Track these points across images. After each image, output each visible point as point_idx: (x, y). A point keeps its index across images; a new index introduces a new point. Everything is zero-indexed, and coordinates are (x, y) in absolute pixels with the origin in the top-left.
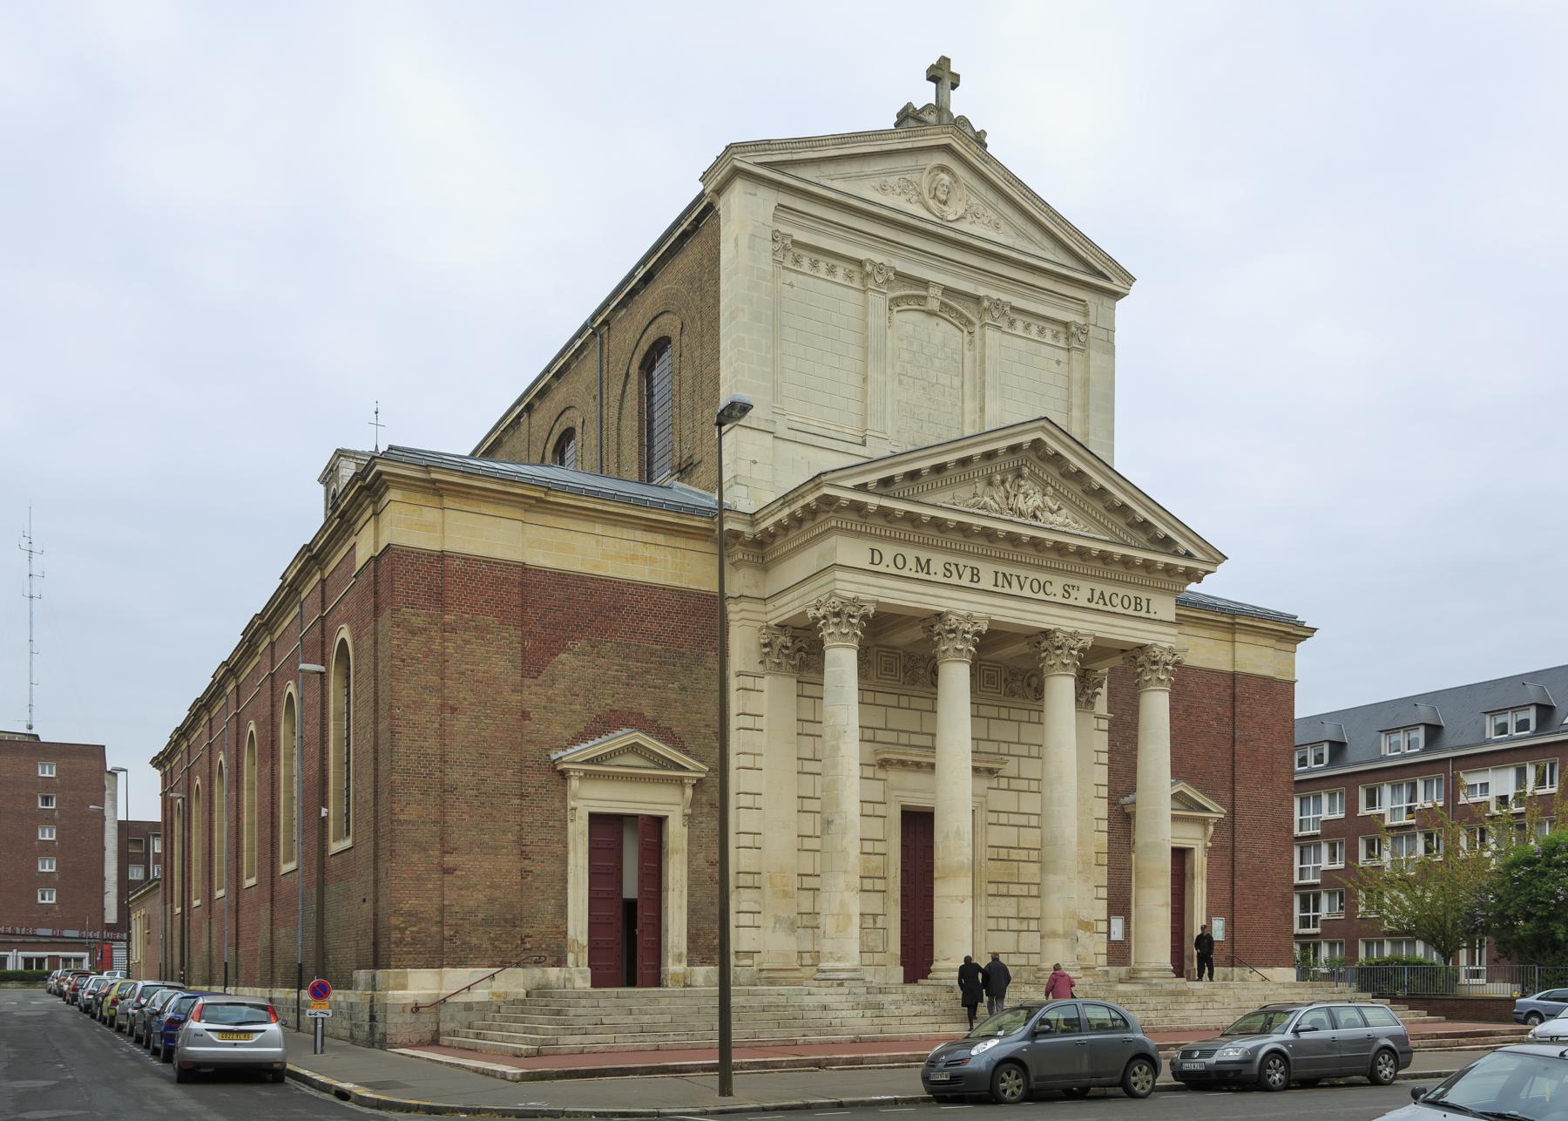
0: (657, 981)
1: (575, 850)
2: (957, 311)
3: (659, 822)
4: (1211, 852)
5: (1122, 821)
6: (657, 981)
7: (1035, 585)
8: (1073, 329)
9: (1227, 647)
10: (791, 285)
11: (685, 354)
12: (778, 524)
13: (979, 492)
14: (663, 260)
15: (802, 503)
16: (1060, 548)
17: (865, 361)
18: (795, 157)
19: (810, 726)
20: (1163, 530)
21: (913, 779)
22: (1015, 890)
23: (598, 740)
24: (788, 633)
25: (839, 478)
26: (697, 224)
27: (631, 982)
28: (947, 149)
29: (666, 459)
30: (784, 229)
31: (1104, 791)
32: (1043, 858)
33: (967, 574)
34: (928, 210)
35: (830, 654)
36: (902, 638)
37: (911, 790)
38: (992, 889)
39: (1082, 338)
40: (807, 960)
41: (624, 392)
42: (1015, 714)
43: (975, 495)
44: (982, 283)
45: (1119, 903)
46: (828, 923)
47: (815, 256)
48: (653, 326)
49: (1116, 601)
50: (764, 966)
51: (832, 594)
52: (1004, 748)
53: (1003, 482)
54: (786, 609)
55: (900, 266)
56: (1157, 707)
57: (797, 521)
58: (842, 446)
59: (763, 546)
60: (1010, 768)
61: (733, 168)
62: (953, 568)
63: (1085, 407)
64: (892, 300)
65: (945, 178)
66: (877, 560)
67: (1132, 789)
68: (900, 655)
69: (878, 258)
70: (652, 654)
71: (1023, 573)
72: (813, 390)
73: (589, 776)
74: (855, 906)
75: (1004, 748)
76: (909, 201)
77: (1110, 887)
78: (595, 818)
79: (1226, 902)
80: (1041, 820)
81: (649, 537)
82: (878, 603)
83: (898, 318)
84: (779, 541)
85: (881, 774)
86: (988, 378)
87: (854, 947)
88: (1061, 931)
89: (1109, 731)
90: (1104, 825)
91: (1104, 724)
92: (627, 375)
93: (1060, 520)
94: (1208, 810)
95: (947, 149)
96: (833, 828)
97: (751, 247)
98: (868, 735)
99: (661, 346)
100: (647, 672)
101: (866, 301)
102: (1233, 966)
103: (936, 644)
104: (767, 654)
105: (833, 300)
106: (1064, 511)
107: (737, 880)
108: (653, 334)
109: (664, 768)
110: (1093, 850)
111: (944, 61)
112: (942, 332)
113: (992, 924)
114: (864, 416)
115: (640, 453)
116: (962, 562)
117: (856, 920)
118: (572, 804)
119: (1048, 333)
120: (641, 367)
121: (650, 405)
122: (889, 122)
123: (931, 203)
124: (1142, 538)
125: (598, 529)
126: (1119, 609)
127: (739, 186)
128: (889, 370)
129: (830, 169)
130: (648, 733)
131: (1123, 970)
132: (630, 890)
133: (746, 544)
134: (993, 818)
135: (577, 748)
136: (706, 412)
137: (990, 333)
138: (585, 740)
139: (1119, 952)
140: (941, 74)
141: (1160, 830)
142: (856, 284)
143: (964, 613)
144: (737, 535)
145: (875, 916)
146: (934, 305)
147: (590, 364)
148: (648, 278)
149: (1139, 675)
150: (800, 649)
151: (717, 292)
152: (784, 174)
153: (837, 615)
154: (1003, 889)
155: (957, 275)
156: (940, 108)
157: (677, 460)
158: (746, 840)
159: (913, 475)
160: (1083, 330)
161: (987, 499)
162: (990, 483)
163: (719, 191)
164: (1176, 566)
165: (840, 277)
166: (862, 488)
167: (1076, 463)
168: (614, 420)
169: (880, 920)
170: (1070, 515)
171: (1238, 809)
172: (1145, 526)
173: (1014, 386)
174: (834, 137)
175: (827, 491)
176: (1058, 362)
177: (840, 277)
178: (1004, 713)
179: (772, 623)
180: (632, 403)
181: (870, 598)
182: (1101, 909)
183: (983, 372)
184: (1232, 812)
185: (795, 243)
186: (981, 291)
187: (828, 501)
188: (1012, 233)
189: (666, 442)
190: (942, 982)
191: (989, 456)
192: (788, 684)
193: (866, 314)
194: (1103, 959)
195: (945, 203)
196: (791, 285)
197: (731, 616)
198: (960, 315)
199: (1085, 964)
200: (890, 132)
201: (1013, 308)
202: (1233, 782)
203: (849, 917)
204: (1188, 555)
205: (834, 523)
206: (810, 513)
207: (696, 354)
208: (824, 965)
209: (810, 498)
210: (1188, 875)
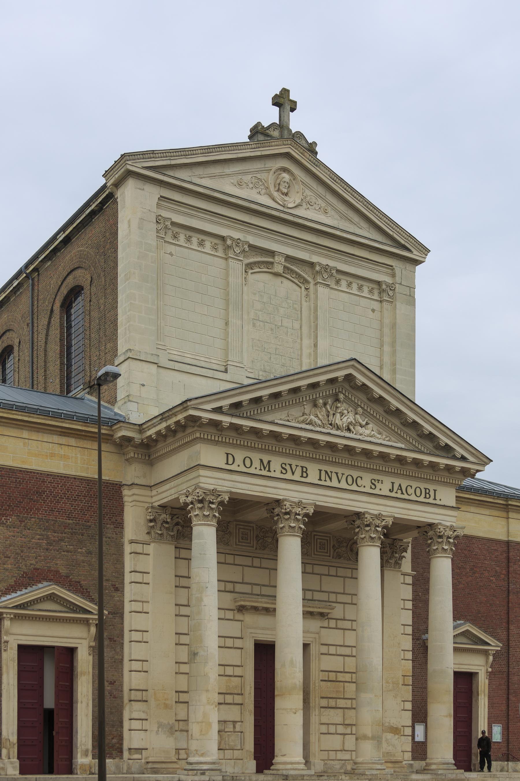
0: (69, 770)
1: (8, 673)
2: (297, 273)
3: (71, 652)
4: (491, 675)
5: (421, 650)
6: (69, 770)
7: (350, 480)
8: (384, 287)
9: (503, 522)
10: (171, 254)
11: (94, 300)
12: (158, 433)
13: (307, 411)
14: (77, 229)
15: (174, 419)
16: (367, 453)
17: (227, 309)
18: (173, 162)
19: (183, 581)
20: (444, 440)
21: (262, 620)
22: (341, 703)
23: (24, 591)
24: (169, 511)
25: (202, 403)
26: (100, 209)
27: (51, 772)
28: (287, 156)
29: (81, 375)
30: (165, 214)
31: (409, 630)
32: (358, 678)
33: (298, 471)
34: (276, 202)
35: (196, 530)
36: (254, 516)
37: (259, 628)
38: (324, 703)
39: (391, 293)
40: (183, 755)
41: (49, 323)
42: (341, 572)
43: (304, 414)
44: (314, 253)
45: (420, 714)
46: (194, 729)
47: (189, 233)
48: (71, 277)
49: (410, 491)
50: (150, 759)
51: (197, 486)
52: (333, 597)
53: (325, 404)
54: (165, 495)
55: (252, 240)
56: (442, 569)
57: (171, 432)
58: (210, 373)
59: (148, 448)
60: (338, 611)
61: (126, 170)
62: (288, 468)
63: (393, 344)
64: (247, 265)
65: (286, 176)
66: (230, 461)
67: (426, 631)
68: (248, 529)
69: (236, 235)
70: (65, 527)
71: (340, 471)
72: (181, 337)
73: (17, 617)
74: (214, 717)
75: (333, 597)
76: (259, 193)
77: (413, 701)
78: (22, 648)
79: (501, 713)
80: (354, 651)
81: (63, 440)
82: (231, 493)
83: (251, 278)
84: (160, 445)
85: (239, 616)
86: (320, 322)
87: (213, 746)
88: (370, 735)
89: (413, 584)
90: (409, 655)
91: (409, 580)
92: (52, 311)
93: (367, 432)
94: (489, 644)
95: (287, 156)
96: (198, 659)
97: (140, 228)
98: (226, 586)
99: (76, 291)
100: (62, 540)
101: (228, 265)
102: (508, 760)
103: (276, 523)
104: (152, 527)
105: (202, 264)
106: (370, 426)
107: (130, 695)
108: (70, 282)
109: (75, 612)
110: (400, 673)
111: (285, 92)
112: (286, 287)
113: (324, 729)
114: (226, 351)
115: (61, 370)
116: (294, 463)
117: (215, 727)
118: (5, 638)
119: (366, 289)
120: (62, 306)
121: (69, 335)
122: (244, 137)
123: (276, 194)
124: (430, 445)
125: (25, 434)
126: (413, 497)
127: (131, 184)
128: (245, 317)
129: (200, 171)
130: (63, 586)
131: (423, 763)
132: (49, 701)
133: (136, 446)
134: (324, 649)
135: (9, 597)
136: (108, 346)
137: (321, 289)
138: (15, 591)
139: (420, 750)
140: (283, 101)
141: (446, 661)
142: (220, 253)
143: (296, 500)
144: (128, 440)
145: (234, 722)
146: (279, 269)
147: (24, 301)
148: (67, 241)
149: (429, 545)
150: (174, 524)
151: (116, 258)
152: (165, 175)
153: (201, 501)
154: (332, 703)
155: (293, 246)
156: (282, 126)
157: (88, 379)
158: (136, 666)
159: (257, 400)
160: (391, 287)
161: (312, 417)
162: (315, 405)
163: (117, 185)
164: (454, 467)
165: (208, 248)
166: (218, 410)
167: (378, 391)
168: (42, 343)
169: (238, 725)
170: (375, 428)
171: (512, 644)
172: (431, 437)
173: (337, 331)
174: (202, 148)
175: (192, 412)
176: (373, 311)
177: (208, 248)
178: (333, 571)
179: (156, 504)
180: (55, 332)
181: (225, 489)
182: (407, 718)
183: (316, 318)
184: (507, 646)
185: (173, 224)
186: (315, 259)
187: (194, 420)
188: (337, 216)
189: (80, 363)
190: (280, 772)
191: (314, 386)
192: (169, 549)
193: (227, 275)
194: (408, 756)
195: (286, 194)
196: (171, 254)
197: (126, 499)
198: (299, 276)
199: (393, 759)
200: (245, 144)
201: (339, 271)
202: (508, 623)
203: (209, 725)
204: (463, 459)
205: (198, 435)
206: (181, 427)
207: (102, 301)
208: (191, 759)
209: (180, 417)
210: (474, 694)
